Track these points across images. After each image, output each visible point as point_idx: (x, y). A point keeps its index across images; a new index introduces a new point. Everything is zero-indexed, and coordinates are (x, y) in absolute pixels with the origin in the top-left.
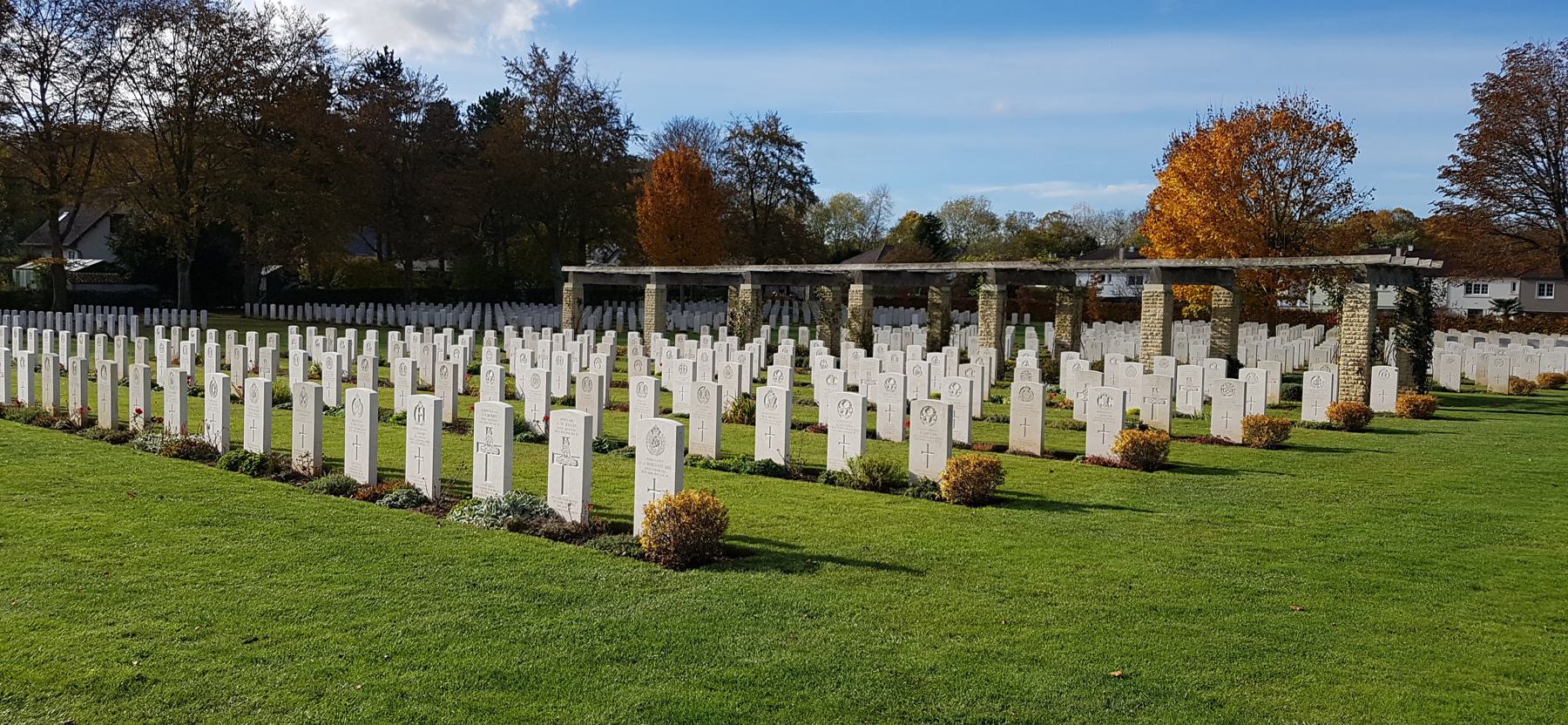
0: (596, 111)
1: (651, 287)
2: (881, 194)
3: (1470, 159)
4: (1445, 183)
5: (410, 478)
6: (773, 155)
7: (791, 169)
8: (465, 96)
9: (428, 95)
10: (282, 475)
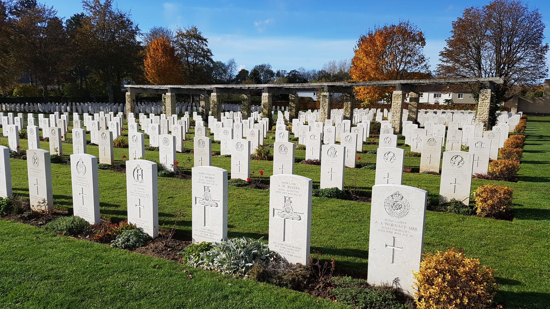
0: (122, 23)
1: (169, 94)
2: (232, 63)
3: (451, 49)
4: (441, 57)
5: (132, 218)
6: (195, 44)
7: (203, 49)
8: (65, 14)
9: (50, 14)
10: (26, 215)
